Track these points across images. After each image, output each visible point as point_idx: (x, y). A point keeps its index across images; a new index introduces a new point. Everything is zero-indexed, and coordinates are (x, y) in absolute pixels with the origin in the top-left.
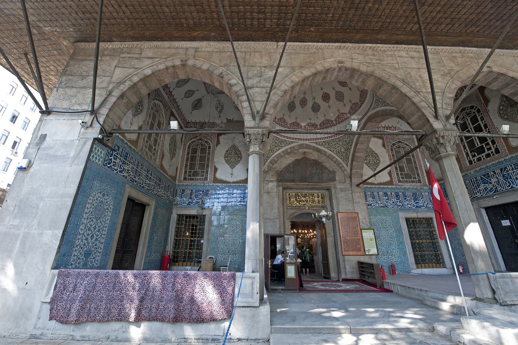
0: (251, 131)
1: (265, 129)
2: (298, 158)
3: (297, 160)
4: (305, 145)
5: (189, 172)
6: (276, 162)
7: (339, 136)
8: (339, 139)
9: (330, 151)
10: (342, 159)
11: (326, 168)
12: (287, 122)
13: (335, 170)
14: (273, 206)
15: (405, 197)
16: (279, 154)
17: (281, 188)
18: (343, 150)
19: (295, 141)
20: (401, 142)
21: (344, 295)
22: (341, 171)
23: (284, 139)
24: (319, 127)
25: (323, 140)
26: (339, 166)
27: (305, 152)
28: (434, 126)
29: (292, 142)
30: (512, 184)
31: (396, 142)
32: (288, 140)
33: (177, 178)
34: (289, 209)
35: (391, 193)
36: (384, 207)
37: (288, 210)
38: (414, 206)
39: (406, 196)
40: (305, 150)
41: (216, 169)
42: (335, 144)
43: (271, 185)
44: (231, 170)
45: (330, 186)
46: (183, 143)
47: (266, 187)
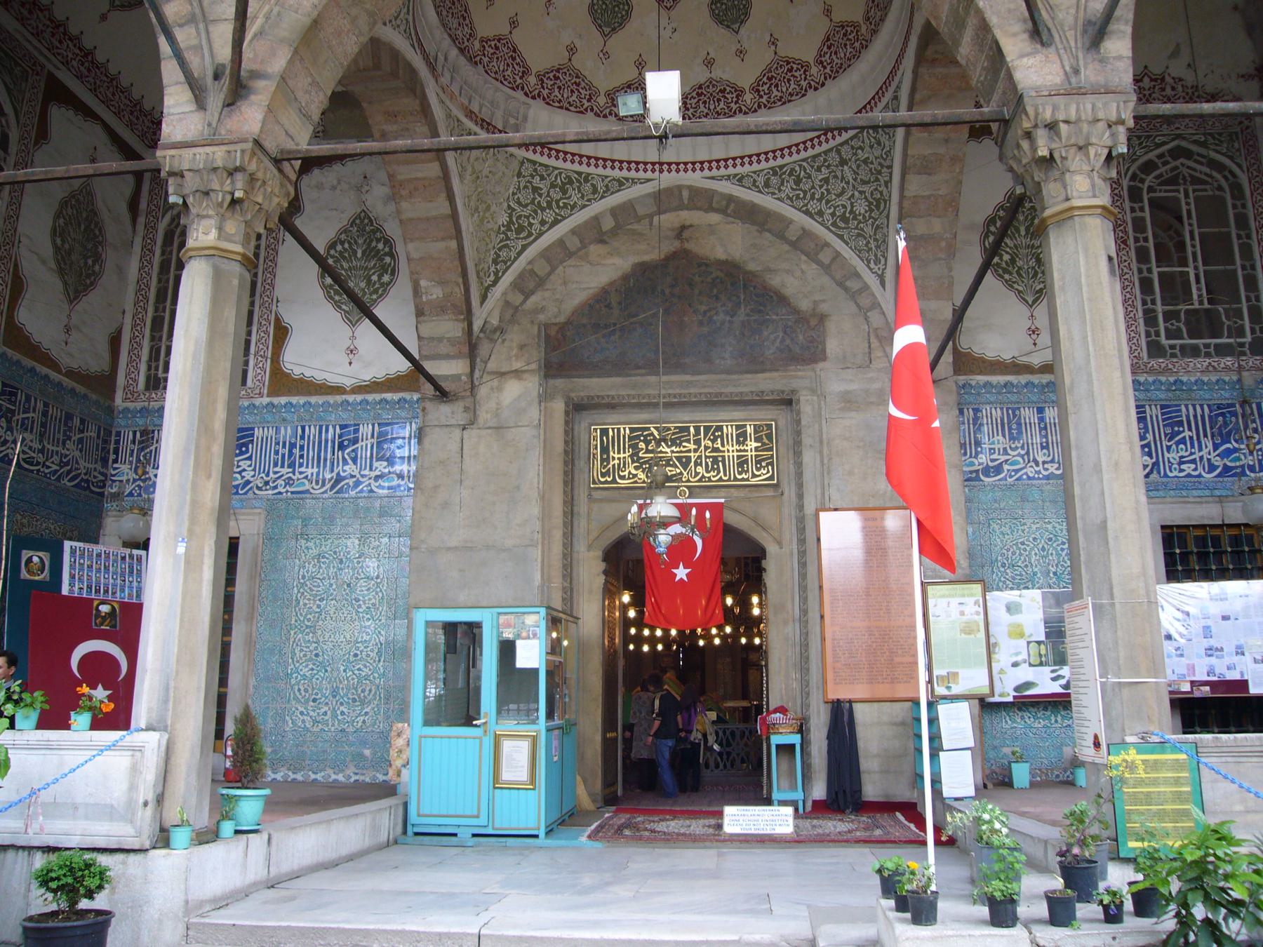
0: (185, 160)
1: (239, 147)
2: (647, 258)
3: (643, 270)
4: (685, 194)
5: (1168, 316)
6: (541, 283)
7: (839, 140)
8: (838, 152)
9: (807, 213)
10: (858, 251)
11: (782, 300)
12: (590, 86)
13: (824, 308)
14: (518, 488)
15: (1172, 425)
16: (561, 242)
17: (559, 406)
18: (861, 207)
19: (633, 174)
20: (1188, 154)
22: (854, 309)
23: (576, 167)
24: (748, 97)
25: (772, 163)
26: (846, 289)
27: (683, 228)
28: (1018, 76)
29: (621, 183)
31: (1160, 156)
32: (600, 171)
33: (121, 379)
34: (601, 500)
37: (595, 507)
38: (1212, 468)
39: (1180, 423)
40: (686, 216)
41: (282, 333)
42: (826, 180)
43: (513, 390)
44: (347, 330)
45: (795, 384)
46: (141, 220)
47: (492, 404)
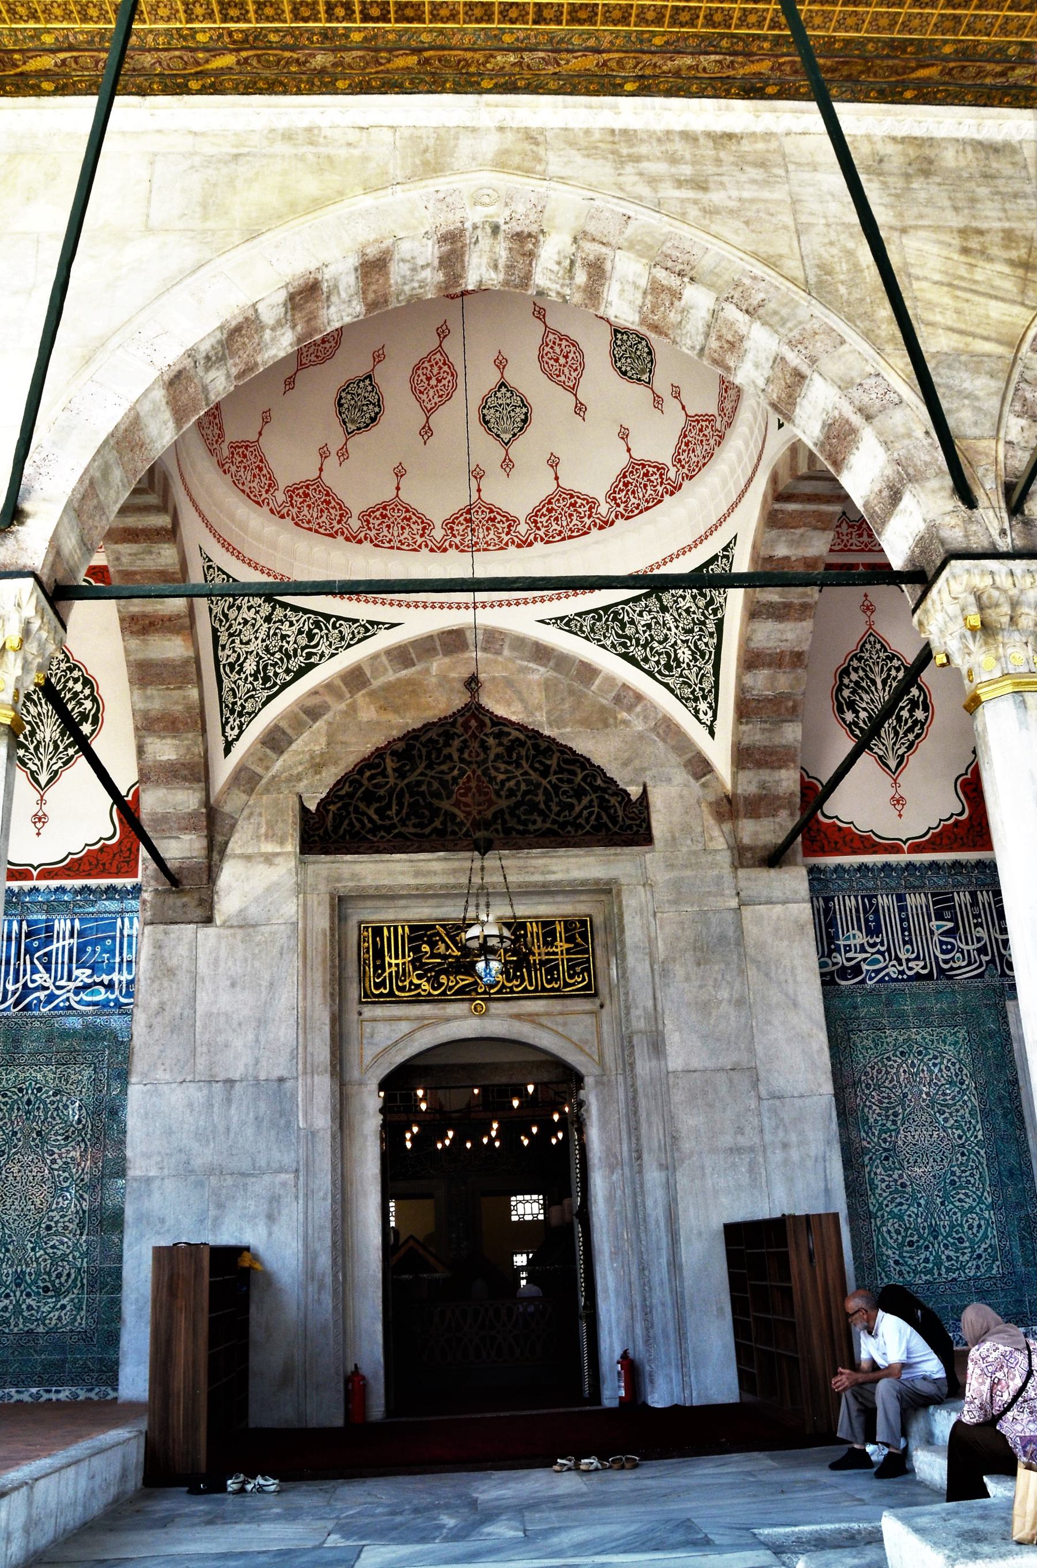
12: (341, 506)
21: (904, 1483)
30: (526, 983)
35: (973, 895)
36: (929, 977)
